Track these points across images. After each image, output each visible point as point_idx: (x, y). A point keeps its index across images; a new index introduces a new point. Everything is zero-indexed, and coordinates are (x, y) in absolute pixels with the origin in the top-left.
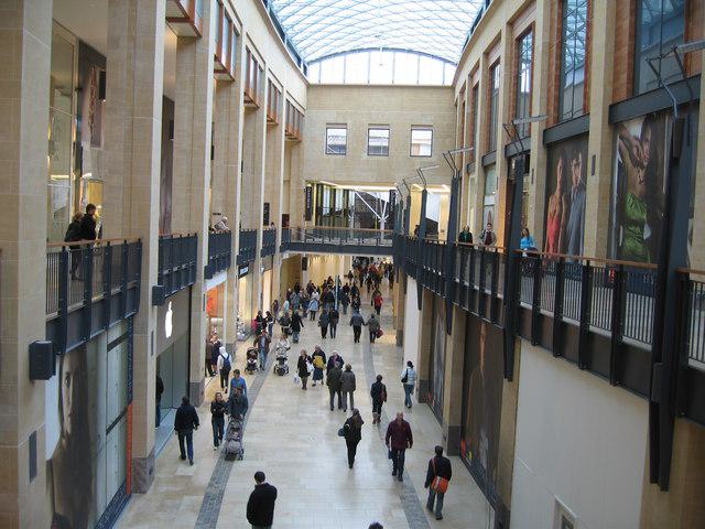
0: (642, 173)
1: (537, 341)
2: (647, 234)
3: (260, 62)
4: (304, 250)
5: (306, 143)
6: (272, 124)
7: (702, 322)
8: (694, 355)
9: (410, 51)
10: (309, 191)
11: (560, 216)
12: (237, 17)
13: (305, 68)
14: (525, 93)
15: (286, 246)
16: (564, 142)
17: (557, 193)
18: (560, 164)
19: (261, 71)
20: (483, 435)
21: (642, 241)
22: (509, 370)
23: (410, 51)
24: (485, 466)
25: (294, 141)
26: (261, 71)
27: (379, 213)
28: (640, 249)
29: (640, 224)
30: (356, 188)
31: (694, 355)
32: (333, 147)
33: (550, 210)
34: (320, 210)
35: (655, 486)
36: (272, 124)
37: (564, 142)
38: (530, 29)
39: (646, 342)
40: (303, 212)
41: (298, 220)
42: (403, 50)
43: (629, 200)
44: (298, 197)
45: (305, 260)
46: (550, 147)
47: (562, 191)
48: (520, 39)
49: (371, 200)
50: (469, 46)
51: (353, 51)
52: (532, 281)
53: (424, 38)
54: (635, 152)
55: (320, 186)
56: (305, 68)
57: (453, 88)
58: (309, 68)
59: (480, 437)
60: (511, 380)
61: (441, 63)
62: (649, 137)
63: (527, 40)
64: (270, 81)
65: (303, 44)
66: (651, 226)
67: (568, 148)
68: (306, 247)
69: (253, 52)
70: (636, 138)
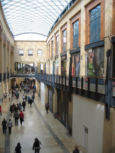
0: (92, 59)
1: (77, 93)
2: (94, 71)
3: (6, 36)
4: (15, 77)
5: (14, 54)
6: (8, 49)
7: (114, 89)
9: (37, 33)
10: (15, 64)
11: (74, 68)
12: (2, 27)
13: (14, 37)
15: (12, 76)
16: (75, 53)
17: (73, 63)
19: (6, 38)
20: (63, 114)
21: (93, 73)
22: (71, 100)
23: (37, 33)
24: (64, 120)
25: (12, 53)
26: (6, 38)
27: (30, 68)
28: (92, 74)
29: (92, 69)
30: (25, 63)
32: (20, 54)
34: (17, 68)
35: (107, 120)
36: (8, 49)
37: (75, 53)
38: (53, 41)
40: (14, 69)
41: (13, 70)
42: (35, 33)
43: (90, 64)
44: (13, 66)
45: (15, 79)
46: (72, 54)
47: (74, 63)
48: (63, 32)
49: (28, 66)
50: (50, 33)
51: (24, 33)
53: (21, 28)
54: (91, 55)
55: (18, 63)
56: (14, 37)
57: (46, 41)
58: (15, 37)
59: (62, 114)
60: (71, 102)
61: (44, 36)
62: (93, 52)
64: (7, 40)
65: (14, 32)
66: (94, 69)
67: (75, 54)
68: (15, 76)
69: (5, 34)
70: (91, 52)
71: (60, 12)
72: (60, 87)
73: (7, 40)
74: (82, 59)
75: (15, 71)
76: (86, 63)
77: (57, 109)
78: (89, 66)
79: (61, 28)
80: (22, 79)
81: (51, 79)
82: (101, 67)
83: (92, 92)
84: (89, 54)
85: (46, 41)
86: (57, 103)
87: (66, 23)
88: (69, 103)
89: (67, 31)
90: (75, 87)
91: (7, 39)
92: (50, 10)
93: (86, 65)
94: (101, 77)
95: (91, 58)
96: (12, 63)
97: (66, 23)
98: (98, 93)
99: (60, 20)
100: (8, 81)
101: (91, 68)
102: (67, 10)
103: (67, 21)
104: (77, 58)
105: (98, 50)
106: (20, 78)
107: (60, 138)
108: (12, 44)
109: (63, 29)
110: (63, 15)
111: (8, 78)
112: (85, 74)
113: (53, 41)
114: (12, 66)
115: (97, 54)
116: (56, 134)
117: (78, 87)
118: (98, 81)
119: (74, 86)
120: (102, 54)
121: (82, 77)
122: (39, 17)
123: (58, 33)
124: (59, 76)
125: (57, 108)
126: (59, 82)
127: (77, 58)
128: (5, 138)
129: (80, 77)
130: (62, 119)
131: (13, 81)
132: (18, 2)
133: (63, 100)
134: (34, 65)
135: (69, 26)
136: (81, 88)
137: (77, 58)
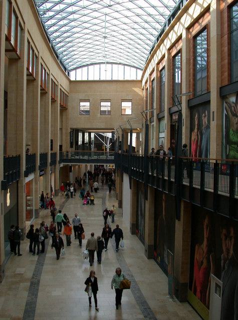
3: (47, 70)
6: (54, 101)
13: (68, 73)
15: (62, 161)
16: (199, 105)
25: (64, 109)
26: (48, 75)
37: (199, 105)
43: (231, 132)
45: (71, 167)
47: (198, 129)
50: (149, 62)
56: (68, 73)
59: (164, 249)
64: (52, 79)
67: (201, 109)
68: (71, 161)
69: (44, 65)
70: (233, 103)
71: (168, 13)
73: (52, 79)
75: (70, 150)
76: (224, 130)
77: (152, 238)
78: (231, 136)
80: (90, 167)
81: (166, 172)
83: (223, 196)
84: (230, 107)
85: (141, 81)
86: (153, 222)
88: (176, 225)
90: (199, 187)
91: (51, 77)
92: (145, 9)
95: (233, 118)
96: (64, 131)
100: (53, 171)
101: (233, 141)
104: (203, 118)
106: (84, 165)
107: (152, 304)
108: (63, 89)
111: (53, 163)
112: (222, 156)
114: (64, 137)
116: (144, 295)
117: (206, 189)
119: (197, 187)
121: (214, 161)
122: (120, 26)
125: (153, 231)
127: (204, 117)
128: (28, 296)
129: (209, 163)
130: (162, 261)
131: (66, 171)
132: (96, 3)
133: (165, 215)
134: (113, 136)
136: (212, 191)
137: (204, 117)
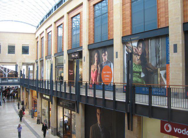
0: (138, 57)
4: (8, 85)
8: (154, 103)
11: (97, 71)
14: (61, 37)
17: (95, 64)
18: (96, 55)
31: (154, 103)
33: (92, 69)
38: (43, 37)
39: (147, 103)
47: (98, 63)
52: (85, 90)
57: (35, 34)
62: (141, 46)
63: (50, 34)
70: (135, 47)
72: (61, 96)
74: (52, 65)
79: (55, 23)
82: (159, 69)
83: (107, 99)
85: (35, 34)
87: (63, 17)
89: (81, 18)
93: (126, 66)
94: (159, 84)
97: (63, 17)
98: (136, 104)
99: (53, 13)
102: (64, 2)
103: (64, 15)
104: (103, 56)
105: (152, 44)
109: (58, 24)
110: (58, 7)
113: (43, 37)
115: (148, 49)
118: (154, 90)
119: (68, 92)
120: (160, 49)
123: (50, 28)
124: (35, 80)
126: (64, 90)
127: (104, 56)
135: (65, 21)
